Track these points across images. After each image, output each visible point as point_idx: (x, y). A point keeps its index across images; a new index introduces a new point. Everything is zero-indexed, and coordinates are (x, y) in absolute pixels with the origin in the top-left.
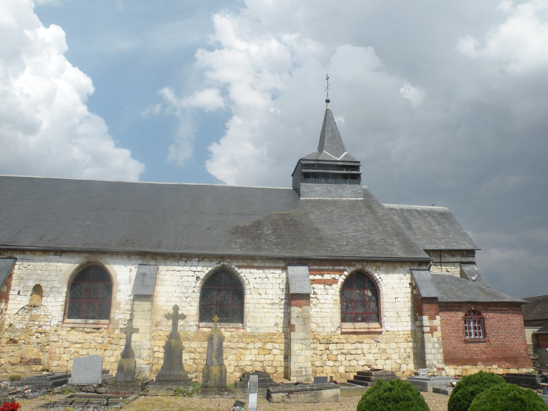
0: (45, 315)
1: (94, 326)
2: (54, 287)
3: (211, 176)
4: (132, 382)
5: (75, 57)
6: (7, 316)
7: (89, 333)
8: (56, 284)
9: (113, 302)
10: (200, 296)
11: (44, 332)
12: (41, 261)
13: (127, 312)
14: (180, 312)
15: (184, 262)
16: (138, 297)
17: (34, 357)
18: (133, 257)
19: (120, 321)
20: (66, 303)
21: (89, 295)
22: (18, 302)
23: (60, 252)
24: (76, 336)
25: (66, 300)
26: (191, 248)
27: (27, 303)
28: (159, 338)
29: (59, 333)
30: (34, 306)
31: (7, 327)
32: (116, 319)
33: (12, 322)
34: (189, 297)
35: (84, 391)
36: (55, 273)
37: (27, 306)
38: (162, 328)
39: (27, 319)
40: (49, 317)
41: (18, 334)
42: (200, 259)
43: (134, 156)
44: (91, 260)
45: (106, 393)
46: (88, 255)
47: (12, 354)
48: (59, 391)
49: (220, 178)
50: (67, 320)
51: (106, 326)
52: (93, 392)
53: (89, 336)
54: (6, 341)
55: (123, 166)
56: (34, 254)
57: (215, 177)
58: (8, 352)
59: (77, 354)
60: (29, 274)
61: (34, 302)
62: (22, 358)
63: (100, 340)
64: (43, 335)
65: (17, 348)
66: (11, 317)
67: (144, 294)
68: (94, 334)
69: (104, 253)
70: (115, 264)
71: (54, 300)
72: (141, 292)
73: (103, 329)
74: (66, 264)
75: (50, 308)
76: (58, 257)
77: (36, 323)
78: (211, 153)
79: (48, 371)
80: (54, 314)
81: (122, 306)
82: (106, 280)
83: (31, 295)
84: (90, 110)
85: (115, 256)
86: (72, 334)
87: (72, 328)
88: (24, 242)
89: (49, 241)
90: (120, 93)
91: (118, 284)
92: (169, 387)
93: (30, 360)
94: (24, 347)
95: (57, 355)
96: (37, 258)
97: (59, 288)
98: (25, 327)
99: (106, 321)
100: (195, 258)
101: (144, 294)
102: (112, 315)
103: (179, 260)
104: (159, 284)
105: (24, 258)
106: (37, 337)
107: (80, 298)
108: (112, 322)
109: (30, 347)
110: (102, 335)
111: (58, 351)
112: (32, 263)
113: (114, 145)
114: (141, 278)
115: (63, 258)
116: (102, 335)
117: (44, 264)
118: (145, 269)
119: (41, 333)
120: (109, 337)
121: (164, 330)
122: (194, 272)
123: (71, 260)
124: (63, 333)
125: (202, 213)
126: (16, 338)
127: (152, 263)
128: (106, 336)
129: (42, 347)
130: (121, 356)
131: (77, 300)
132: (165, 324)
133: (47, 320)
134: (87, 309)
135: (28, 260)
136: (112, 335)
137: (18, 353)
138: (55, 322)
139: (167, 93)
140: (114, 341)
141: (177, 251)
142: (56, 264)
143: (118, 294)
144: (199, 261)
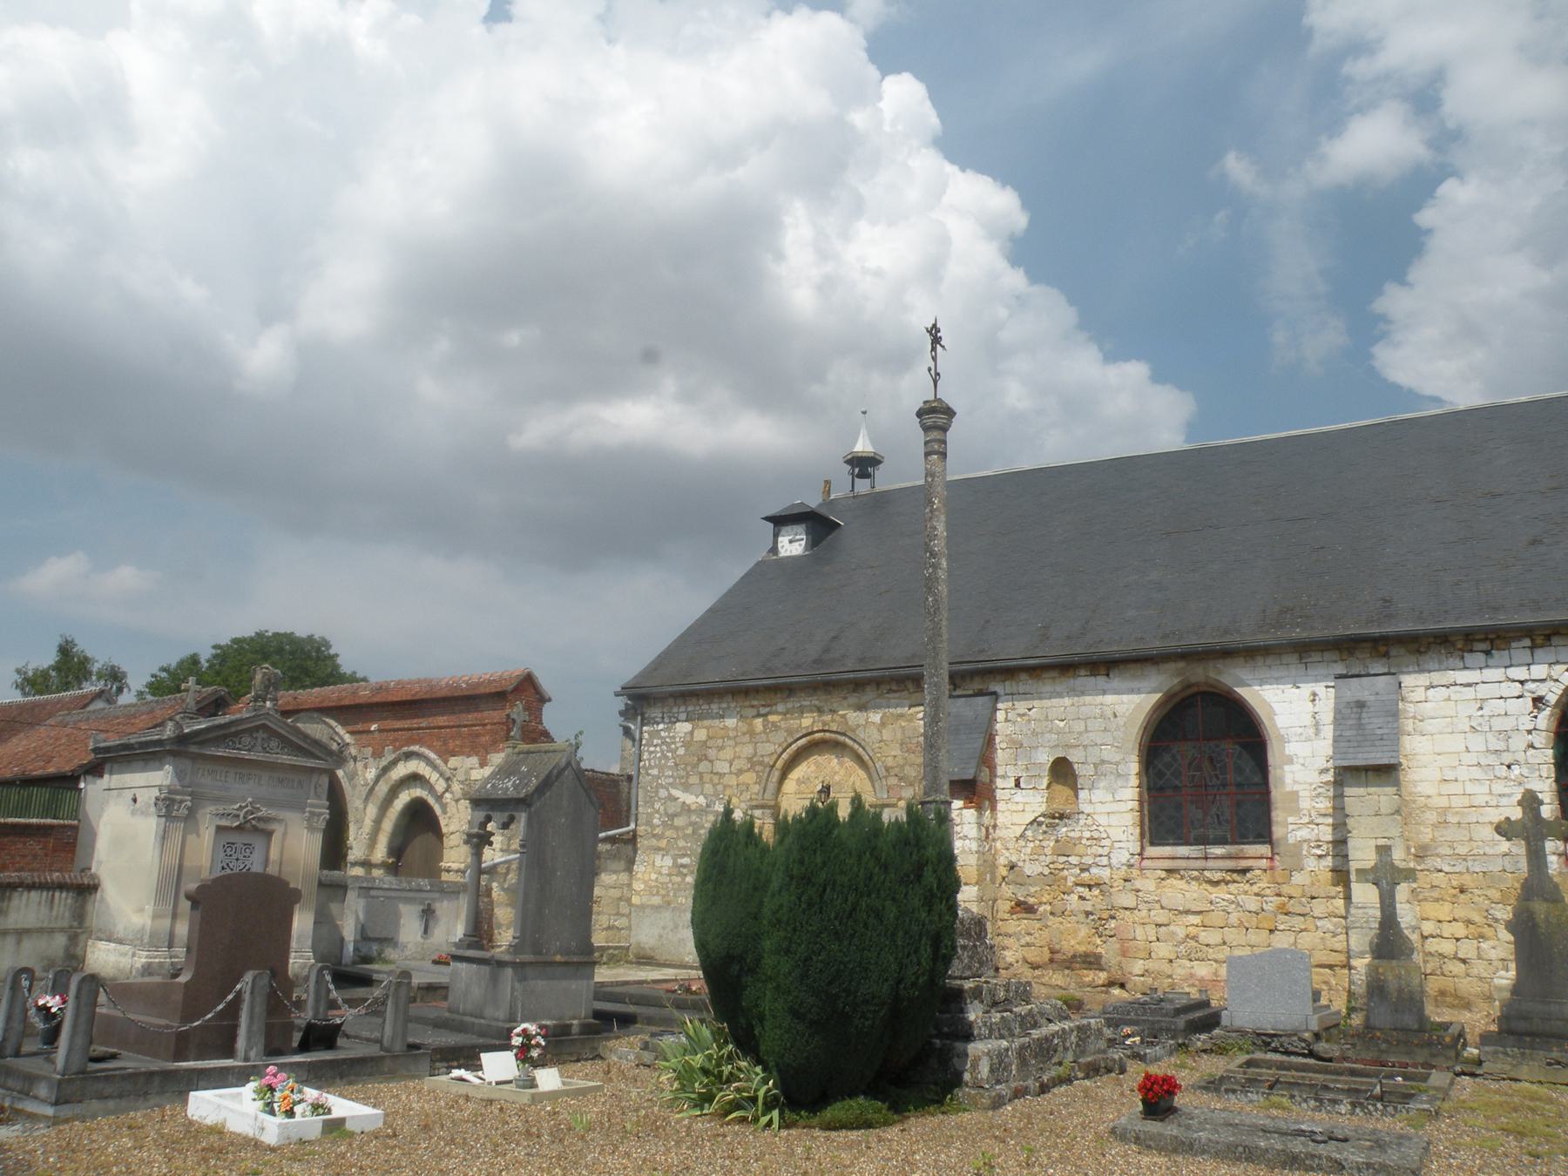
0: (1092, 838)
1: (1231, 864)
2: (1103, 762)
3: (1397, 388)
4: (1421, 1030)
5: (962, 145)
6: (998, 844)
7: (1217, 883)
8: (1108, 753)
9: (1276, 794)
10: (1555, 757)
11: (1098, 885)
12: (1060, 695)
13: (1320, 820)
14: (1516, 814)
15: (1482, 657)
16: (1348, 774)
17: (1082, 949)
18: (1316, 657)
19: (1305, 846)
20: (1141, 802)
21: (1205, 775)
22: (1020, 807)
23: (1104, 666)
24: (1183, 892)
25: (1141, 794)
26: (1496, 609)
27: (1043, 808)
28: (1435, 894)
29: (1138, 884)
30: (1061, 817)
31: (1004, 872)
32: (1291, 841)
33: (1014, 859)
34: (1517, 763)
35: (1275, 1050)
36: (1098, 724)
37: (1043, 815)
38: (1438, 863)
39: (1048, 851)
40: (1103, 843)
41: (1033, 890)
42: (1539, 641)
43: (1158, 377)
44: (1193, 680)
45: (1345, 1059)
46: (1181, 664)
47: (1028, 938)
48: (1208, 1046)
49: (1429, 389)
50: (1152, 851)
51: (1264, 863)
52: (1304, 1055)
53: (1219, 894)
54: (1007, 906)
55: (1133, 411)
56: (1038, 677)
57: (1410, 391)
58: (1017, 936)
59: (1193, 943)
60: (1035, 733)
61: (1058, 806)
62: (1053, 952)
63: (1252, 904)
64: (1096, 892)
65: (1037, 925)
66: (1010, 845)
67: (1367, 769)
68: (1232, 887)
69: (1227, 654)
70: (1262, 682)
71: (1110, 798)
72: (1361, 760)
73: (1258, 872)
74: (1125, 698)
75: (1102, 820)
76: (1091, 681)
77: (1074, 860)
78: (1384, 318)
79: (1122, 986)
80: (1117, 834)
81: (1305, 804)
82: (1248, 736)
83: (1048, 787)
84: (1034, 277)
85: (1260, 660)
86: (1172, 886)
87: (1170, 871)
88: (1011, 650)
89: (1068, 638)
90: (1108, 203)
91: (1283, 740)
92: (1555, 1054)
93: (1074, 956)
94: (1052, 921)
95: (1141, 944)
96: (1047, 687)
97: (1117, 764)
98: (1046, 871)
99: (1264, 849)
100: (1519, 639)
101: (1367, 769)
102: (1277, 831)
103: (1462, 650)
104: (1410, 728)
105: (1014, 690)
106: (1081, 898)
107: (1176, 787)
108: (1281, 849)
109: (1068, 924)
110: (1255, 889)
111: (1140, 933)
112: (1036, 703)
113: (1100, 356)
114: (1350, 717)
115: (1116, 682)
116: (1255, 889)
117: (1067, 701)
118: (1359, 689)
119: (1090, 887)
120: (1279, 895)
121: (1447, 868)
122: (1522, 683)
123: (1136, 684)
124: (1147, 884)
125: (1494, 496)
126: (1031, 900)
127: (1378, 667)
128: (1268, 892)
129: (1098, 923)
130: (1373, 952)
131: (1169, 792)
132: (1449, 851)
133: (1100, 851)
134: (1200, 816)
135: (1026, 695)
136: (1285, 889)
137: (1041, 937)
138: (1121, 857)
139: (1237, 168)
140: (1293, 906)
141: (1449, 624)
142: (1099, 699)
143: (1287, 768)
144: (1532, 648)
